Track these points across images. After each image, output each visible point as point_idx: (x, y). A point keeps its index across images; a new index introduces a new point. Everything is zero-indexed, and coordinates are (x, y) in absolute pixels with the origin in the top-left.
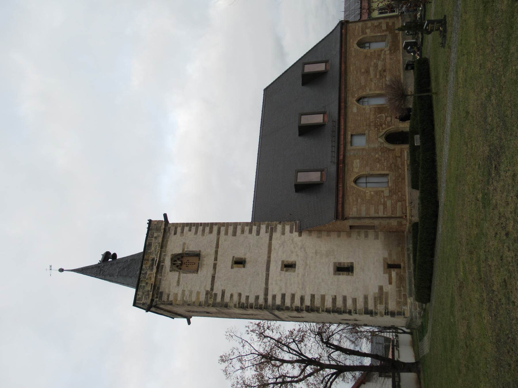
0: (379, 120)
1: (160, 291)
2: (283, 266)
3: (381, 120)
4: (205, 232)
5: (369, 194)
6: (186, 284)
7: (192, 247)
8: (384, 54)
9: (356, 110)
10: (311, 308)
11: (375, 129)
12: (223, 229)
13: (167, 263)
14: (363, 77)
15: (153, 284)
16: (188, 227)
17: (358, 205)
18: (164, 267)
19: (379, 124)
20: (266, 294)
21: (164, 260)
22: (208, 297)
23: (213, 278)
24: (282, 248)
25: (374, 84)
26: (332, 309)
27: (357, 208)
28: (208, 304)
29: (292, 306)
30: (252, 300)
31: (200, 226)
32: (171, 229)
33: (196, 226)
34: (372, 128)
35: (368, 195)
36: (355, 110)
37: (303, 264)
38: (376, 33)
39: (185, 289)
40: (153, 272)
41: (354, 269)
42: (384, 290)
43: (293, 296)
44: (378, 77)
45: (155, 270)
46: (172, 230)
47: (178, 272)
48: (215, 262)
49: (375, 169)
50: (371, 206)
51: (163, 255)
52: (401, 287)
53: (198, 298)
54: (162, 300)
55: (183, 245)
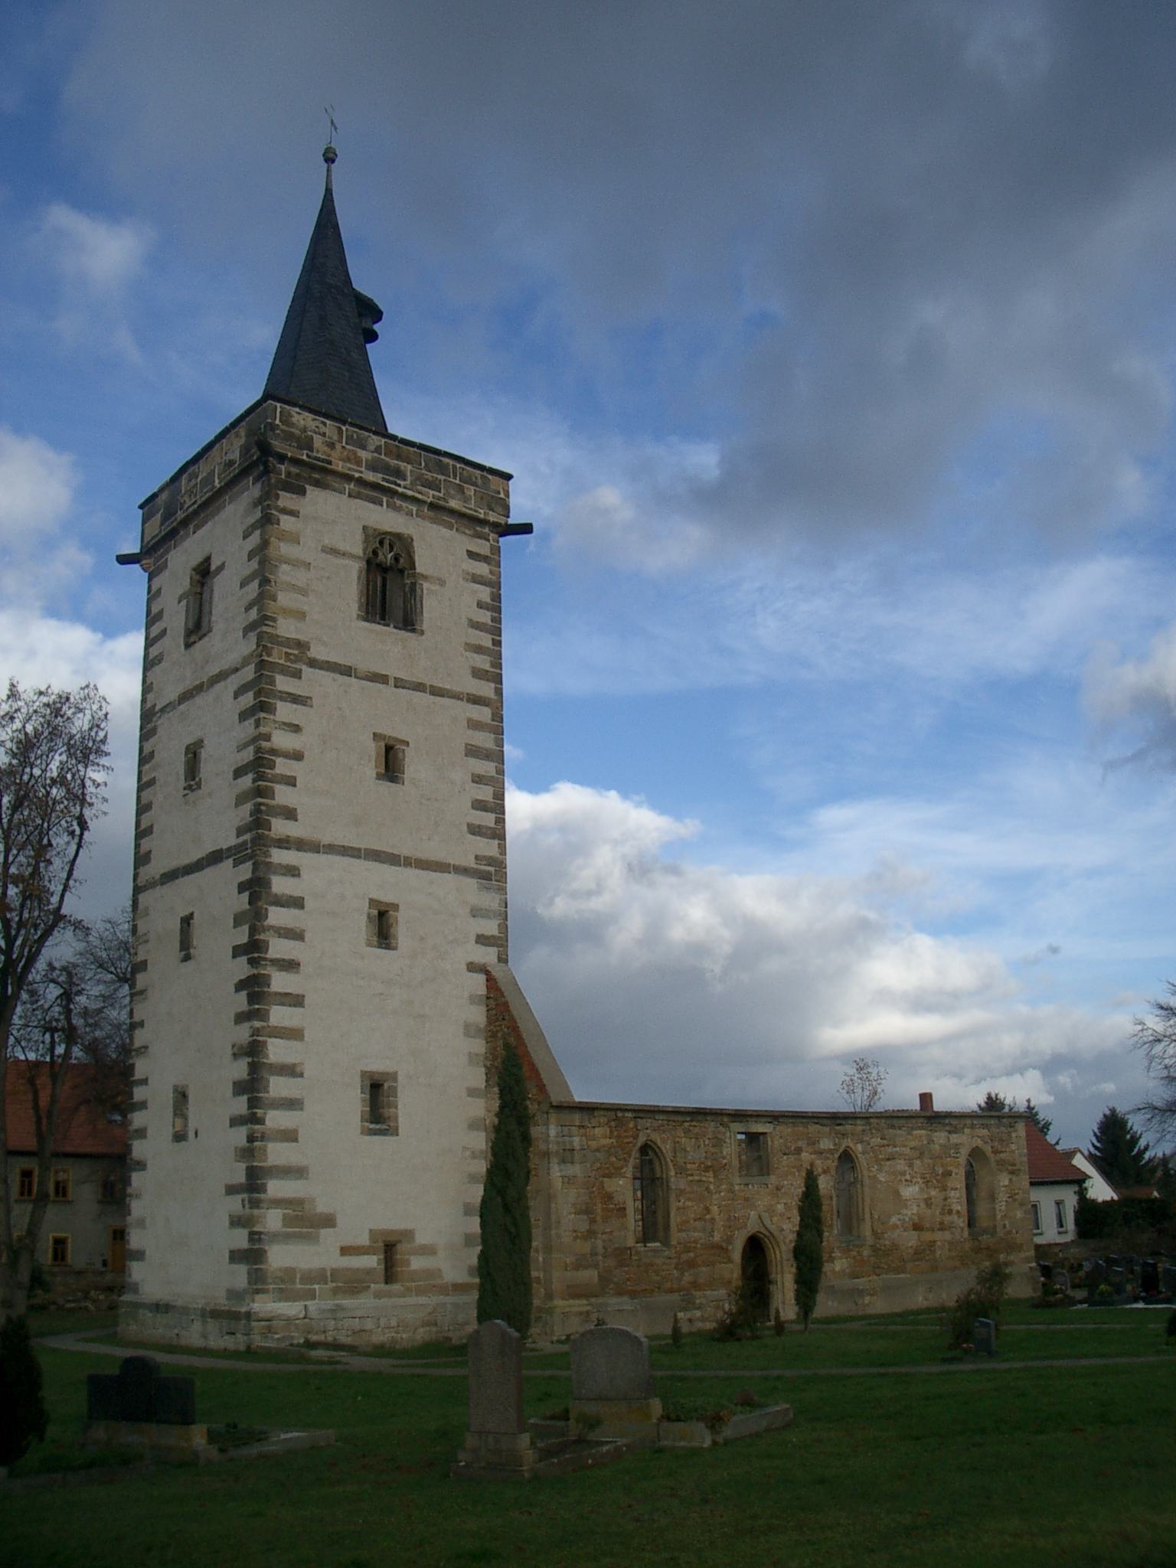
1: (307, 487)
2: (383, 908)
6: (328, 578)
7: (433, 606)
10: (264, 992)
12: (484, 714)
13: (386, 519)
15: (329, 466)
20: (301, 845)
21: (398, 509)
23: (347, 671)
26: (265, 1061)
30: (283, 795)
31: (493, 639)
32: (484, 542)
42: (323, 1231)
43: (297, 935)
45: (371, 477)
48: (392, 682)
51: (410, 507)
52: (334, 1285)
53: (288, 612)
55: (439, 579)
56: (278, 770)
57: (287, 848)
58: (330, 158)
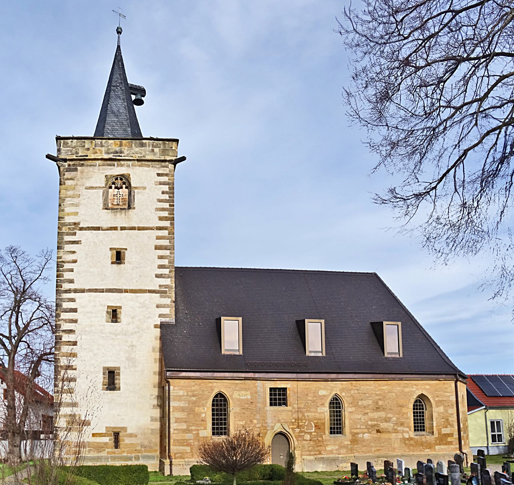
0: (306, 424)
3: (306, 427)
4: (160, 212)
5: (202, 411)
6: (88, 198)
8: (403, 430)
9: (322, 394)
11: (293, 418)
13: (117, 170)
14: (371, 403)
16: (168, 190)
17: (187, 397)
18: (112, 167)
19: (300, 424)
20: (76, 291)
21: (122, 166)
22: (70, 225)
23: (98, 229)
24: (138, 305)
25: (359, 417)
27: (184, 395)
28: (61, 227)
29: (61, 320)
30: (67, 275)
31: (170, 205)
33: (169, 200)
34: (295, 416)
35: (201, 409)
36: (322, 393)
37: (116, 331)
38: (436, 420)
39: (81, 197)
40: (103, 154)
41: (112, 392)
44: (369, 423)
45: (106, 156)
46: (164, 170)
47: (104, 186)
48: (119, 228)
49: (237, 419)
50: (186, 413)
52: (89, 449)
54: (66, 172)
56: (65, 268)
57: (69, 293)
58: (119, 32)
